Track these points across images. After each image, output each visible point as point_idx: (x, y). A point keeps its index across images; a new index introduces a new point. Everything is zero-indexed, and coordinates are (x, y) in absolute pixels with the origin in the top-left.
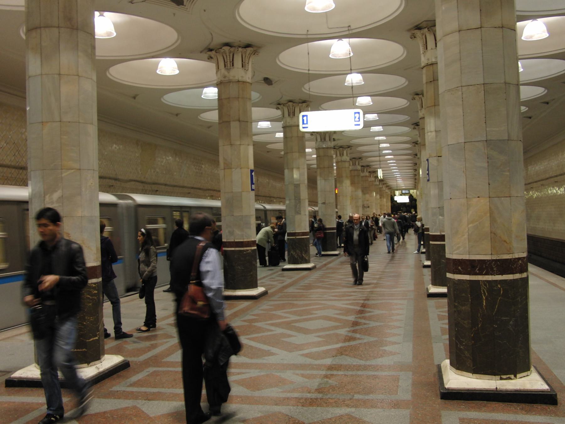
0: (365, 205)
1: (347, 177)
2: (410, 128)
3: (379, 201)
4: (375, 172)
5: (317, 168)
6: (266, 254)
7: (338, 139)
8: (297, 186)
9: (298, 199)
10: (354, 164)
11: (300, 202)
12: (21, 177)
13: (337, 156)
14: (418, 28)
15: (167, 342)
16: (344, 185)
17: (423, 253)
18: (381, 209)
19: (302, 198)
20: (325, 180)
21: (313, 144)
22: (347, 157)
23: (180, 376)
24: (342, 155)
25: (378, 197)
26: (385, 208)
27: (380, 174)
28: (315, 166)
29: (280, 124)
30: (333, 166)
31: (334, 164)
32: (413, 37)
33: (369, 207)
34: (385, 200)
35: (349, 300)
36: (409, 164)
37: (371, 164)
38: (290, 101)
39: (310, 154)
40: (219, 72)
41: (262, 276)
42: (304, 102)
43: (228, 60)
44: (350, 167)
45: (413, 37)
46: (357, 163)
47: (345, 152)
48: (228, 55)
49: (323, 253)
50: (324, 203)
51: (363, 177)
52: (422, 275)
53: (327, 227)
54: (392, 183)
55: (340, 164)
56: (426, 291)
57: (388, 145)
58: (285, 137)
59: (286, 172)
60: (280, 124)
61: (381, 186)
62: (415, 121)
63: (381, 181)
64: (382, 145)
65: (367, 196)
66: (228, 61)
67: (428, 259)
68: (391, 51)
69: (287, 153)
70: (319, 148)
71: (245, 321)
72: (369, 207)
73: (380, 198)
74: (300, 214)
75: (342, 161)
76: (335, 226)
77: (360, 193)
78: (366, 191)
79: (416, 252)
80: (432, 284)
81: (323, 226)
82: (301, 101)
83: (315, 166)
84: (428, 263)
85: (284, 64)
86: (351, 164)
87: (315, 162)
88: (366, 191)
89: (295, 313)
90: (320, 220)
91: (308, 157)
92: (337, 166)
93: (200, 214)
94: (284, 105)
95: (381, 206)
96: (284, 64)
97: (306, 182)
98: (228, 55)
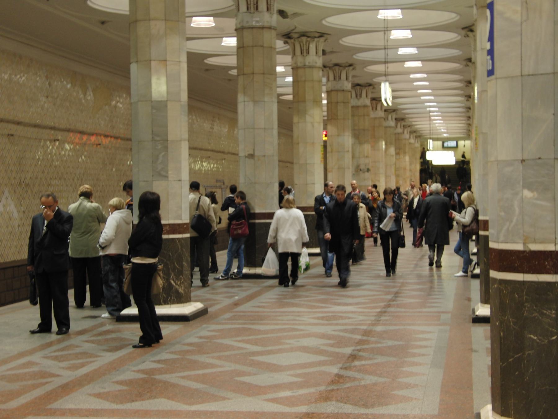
0: (362, 167)
2: (459, 34)
3: (394, 159)
4: (374, 87)
5: (238, 75)
7: (295, 15)
8: (160, 107)
9: (161, 139)
10: (337, 78)
11: (166, 148)
13: (328, 80)
15: (47, 383)
16: (308, 118)
17: (479, 320)
18: (397, 176)
19: (170, 138)
20: (255, 102)
21: (288, 59)
22: (267, 16)
25: (392, 150)
26: (408, 174)
27: (386, 93)
28: (290, 97)
29: (231, 23)
30: (321, 99)
31: (323, 95)
33: (368, 170)
34: (407, 158)
36: (454, 82)
39: (284, 75)
40: (295, 58)
41: (80, 329)
42: (351, 65)
43: (358, 93)
44: (330, 83)
46: (343, 76)
47: (312, 47)
48: (305, 43)
49: (245, 270)
50: (251, 156)
51: (386, 127)
52: (467, 288)
53: (258, 210)
54: (421, 125)
55: (300, 71)
56: (471, 312)
57: (418, 64)
58: (241, 47)
59: (134, 68)
60: (231, 23)
61: (399, 130)
62: (467, 23)
63: (388, 111)
64: (409, 64)
65: (367, 147)
66: (252, 3)
67: (485, 300)
70: (243, 28)
71: (159, 362)
72: (368, 170)
73: (397, 154)
74: (167, 177)
75: (304, 67)
76: (186, 219)
77: (348, 140)
79: (461, 273)
80: (482, 302)
81: (248, 209)
82: (347, 65)
83: (290, 97)
84: (484, 310)
86: (331, 78)
87: (290, 90)
89: (255, 343)
90: (242, 196)
91: (279, 81)
92: (328, 99)
94: (330, 68)
95: (397, 169)
97: (184, 96)
98: (305, 43)
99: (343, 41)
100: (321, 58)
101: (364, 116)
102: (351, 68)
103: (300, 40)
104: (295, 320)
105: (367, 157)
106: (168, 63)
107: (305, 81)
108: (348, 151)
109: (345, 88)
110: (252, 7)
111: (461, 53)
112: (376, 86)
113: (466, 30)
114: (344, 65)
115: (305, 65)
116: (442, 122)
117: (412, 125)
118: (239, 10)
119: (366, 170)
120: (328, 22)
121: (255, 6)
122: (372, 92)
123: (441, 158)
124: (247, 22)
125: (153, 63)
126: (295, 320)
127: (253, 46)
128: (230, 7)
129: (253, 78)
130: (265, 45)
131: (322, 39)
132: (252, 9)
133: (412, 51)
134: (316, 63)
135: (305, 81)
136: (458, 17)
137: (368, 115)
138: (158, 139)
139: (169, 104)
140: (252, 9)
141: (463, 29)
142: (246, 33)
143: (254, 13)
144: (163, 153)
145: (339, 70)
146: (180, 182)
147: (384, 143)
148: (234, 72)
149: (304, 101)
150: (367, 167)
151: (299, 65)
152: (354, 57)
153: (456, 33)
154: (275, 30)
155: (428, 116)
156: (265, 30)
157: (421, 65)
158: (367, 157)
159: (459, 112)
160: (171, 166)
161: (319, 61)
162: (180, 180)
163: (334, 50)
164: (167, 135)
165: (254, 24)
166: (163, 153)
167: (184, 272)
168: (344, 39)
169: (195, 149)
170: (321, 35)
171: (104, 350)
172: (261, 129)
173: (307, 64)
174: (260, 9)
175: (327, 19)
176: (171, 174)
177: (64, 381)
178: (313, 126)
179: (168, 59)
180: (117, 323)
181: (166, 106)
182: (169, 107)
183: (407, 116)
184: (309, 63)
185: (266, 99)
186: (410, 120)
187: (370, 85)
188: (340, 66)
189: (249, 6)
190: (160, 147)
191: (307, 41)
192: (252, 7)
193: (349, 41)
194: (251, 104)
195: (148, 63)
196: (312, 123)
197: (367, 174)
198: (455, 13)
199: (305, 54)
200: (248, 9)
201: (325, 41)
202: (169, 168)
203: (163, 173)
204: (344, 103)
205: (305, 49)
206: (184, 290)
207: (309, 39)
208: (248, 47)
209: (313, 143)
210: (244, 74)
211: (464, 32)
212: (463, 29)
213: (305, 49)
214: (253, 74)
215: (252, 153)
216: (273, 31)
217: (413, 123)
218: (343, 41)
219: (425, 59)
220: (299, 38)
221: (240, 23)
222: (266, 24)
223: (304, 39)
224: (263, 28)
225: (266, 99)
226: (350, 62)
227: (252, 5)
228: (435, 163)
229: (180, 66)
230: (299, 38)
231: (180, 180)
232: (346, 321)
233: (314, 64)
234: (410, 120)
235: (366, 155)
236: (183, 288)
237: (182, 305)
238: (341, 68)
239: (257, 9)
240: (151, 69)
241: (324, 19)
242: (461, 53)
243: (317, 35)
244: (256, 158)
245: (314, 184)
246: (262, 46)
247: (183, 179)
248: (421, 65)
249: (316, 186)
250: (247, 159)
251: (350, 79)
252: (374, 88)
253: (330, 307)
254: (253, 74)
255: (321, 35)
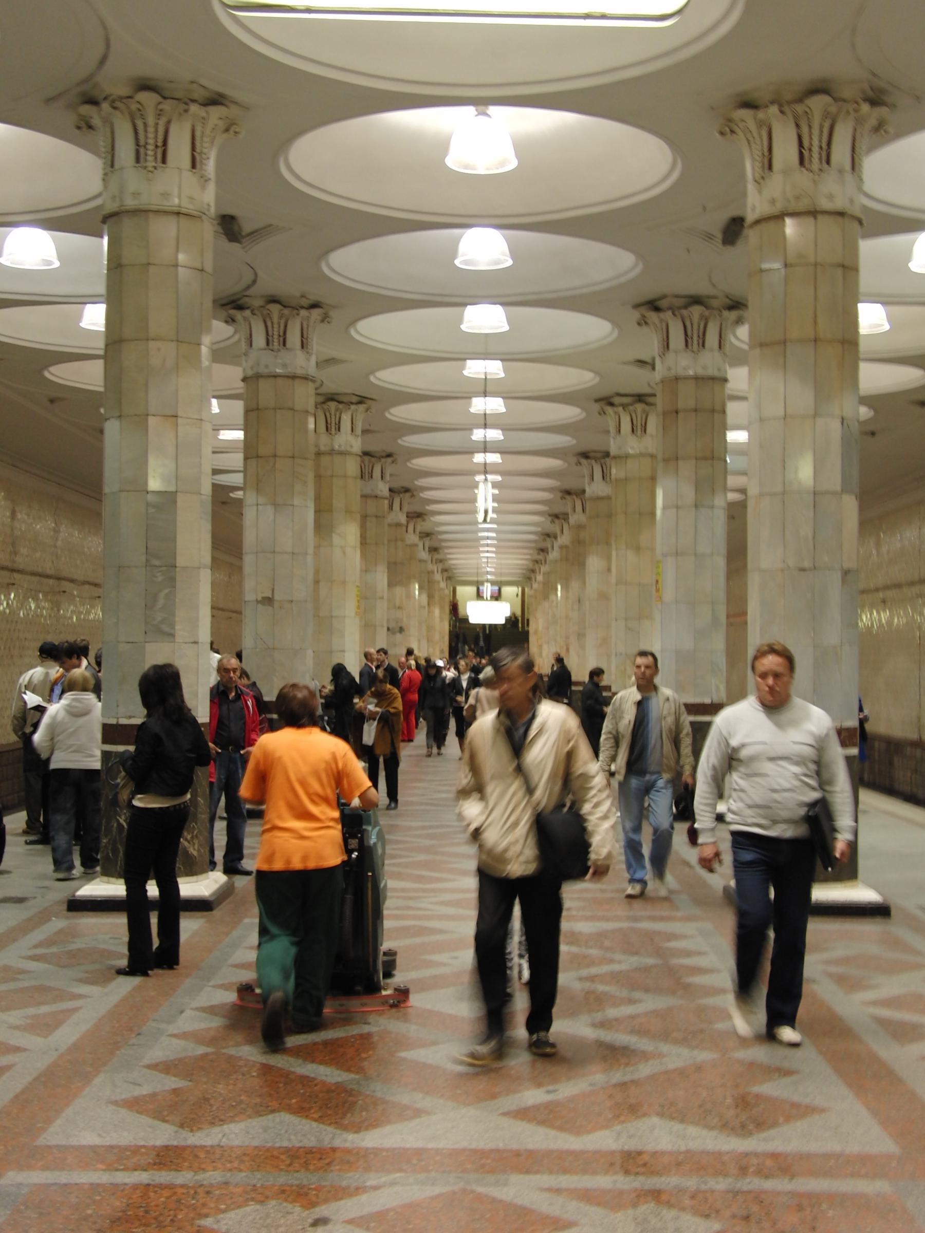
1: (349, 512)
6: (208, 738)
9: (163, 566)
11: (173, 580)
12: (732, 1112)
14: (653, 305)
16: (336, 540)
19: (181, 561)
20: (275, 505)
22: (351, 438)
23: (126, 928)
24: (332, 427)
25: (425, 598)
29: (238, 407)
32: (728, 129)
33: (401, 630)
35: (453, 891)
37: (437, 529)
38: (145, 86)
42: (389, 455)
45: (728, 129)
47: (346, 419)
54: (459, 559)
55: (325, 460)
68: (634, 160)
69: (121, 341)
70: (258, 376)
72: (401, 630)
74: (172, 635)
75: (332, 452)
77: (381, 577)
78: (398, 574)
82: (384, 454)
85: (366, 337)
88: (398, 574)
93: (520, 972)
96: (366, 337)
98: (333, 413)
99: (390, 413)
100: (360, 439)
101: (396, 540)
102: (389, 460)
103: (325, 406)
104: (409, 908)
105: (399, 608)
106: (180, 420)
107: (332, 476)
108: (382, 598)
109: (379, 493)
110: (276, 340)
111: (574, 442)
112: (415, 493)
113: (602, 403)
114: (377, 455)
115: (333, 450)
116: (493, 555)
117: (446, 560)
118: (251, 345)
119: (398, 629)
120: (380, 380)
121: (281, 339)
122: (409, 503)
123: (486, 612)
124: (267, 366)
125: (152, 421)
126: (409, 908)
127: (275, 409)
128: (223, 341)
129: (275, 464)
130: (297, 408)
131: (362, 407)
132: (276, 344)
133: (494, 435)
134: (352, 447)
135: (332, 476)
136: (597, 379)
137: (403, 540)
138: (157, 562)
139: (180, 499)
140: (276, 344)
141: (597, 401)
142: (263, 385)
143: (279, 350)
144: (166, 591)
145: (370, 461)
146: (195, 645)
147: (417, 587)
148: (239, 494)
149: (330, 511)
150: (400, 625)
151: (323, 448)
152: (400, 441)
153: (578, 406)
154: (313, 381)
155: (474, 543)
156: (297, 381)
157: (500, 461)
158: (399, 608)
159: (523, 541)
160: (181, 614)
161: (357, 445)
162: (196, 643)
163: (372, 428)
164: (175, 559)
165: (279, 371)
166: (166, 591)
167: (199, 816)
168: (393, 411)
169: (219, 609)
170: (362, 400)
171: (80, 980)
172: (286, 553)
173: (336, 447)
174: (288, 344)
175: (378, 374)
176: (181, 631)
177: (41, 1064)
178: (344, 553)
179: (180, 414)
180: (70, 914)
181: (175, 502)
182: (179, 504)
183: (444, 544)
184: (340, 446)
185: (296, 502)
186: (446, 551)
187: (407, 490)
188: (373, 456)
189: (270, 338)
190: (160, 579)
191: (337, 410)
192: (276, 340)
193: (401, 413)
194: (270, 510)
195: (141, 420)
196: (343, 548)
197: (398, 635)
198: (591, 371)
199: (333, 431)
200: (268, 344)
201: (367, 410)
202: (177, 619)
203: (165, 628)
204: (376, 517)
205: (333, 422)
206: (199, 851)
207: (341, 406)
208: (266, 409)
209: (344, 583)
210: (258, 457)
211: (597, 407)
212: (597, 401)
213: (333, 422)
214: (275, 456)
215: (268, 594)
216: (310, 384)
217: (449, 556)
218: (390, 413)
219: (516, 450)
220: (323, 403)
221: (252, 368)
222: (299, 372)
223: (333, 405)
224: (293, 377)
225: (296, 502)
226: (389, 449)
227: (276, 337)
228: (472, 620)
229: (200, 428)
230: (323, 403)
231: (196, 643)
232: (447, 897)
233: (349, 449)
234: (446, 551)
235: (398, 604)
236: (196, 847)
237: (194, 878)
238: (373, 459)
239: (284, 345)
240: (147, 430)
241: (372, 372)
242: (574, 442)
243: (355, 399)
244: (276, 605)
245: (344, 651)
246: (292, 409)
247: (200, 641)
248: (500, 461)
249: (346, 654)
250: (260, 606)
251: (388, 477)
252: (413, 496)
253: (450, 880)
254: (275, 456)
255: (362, 400)
